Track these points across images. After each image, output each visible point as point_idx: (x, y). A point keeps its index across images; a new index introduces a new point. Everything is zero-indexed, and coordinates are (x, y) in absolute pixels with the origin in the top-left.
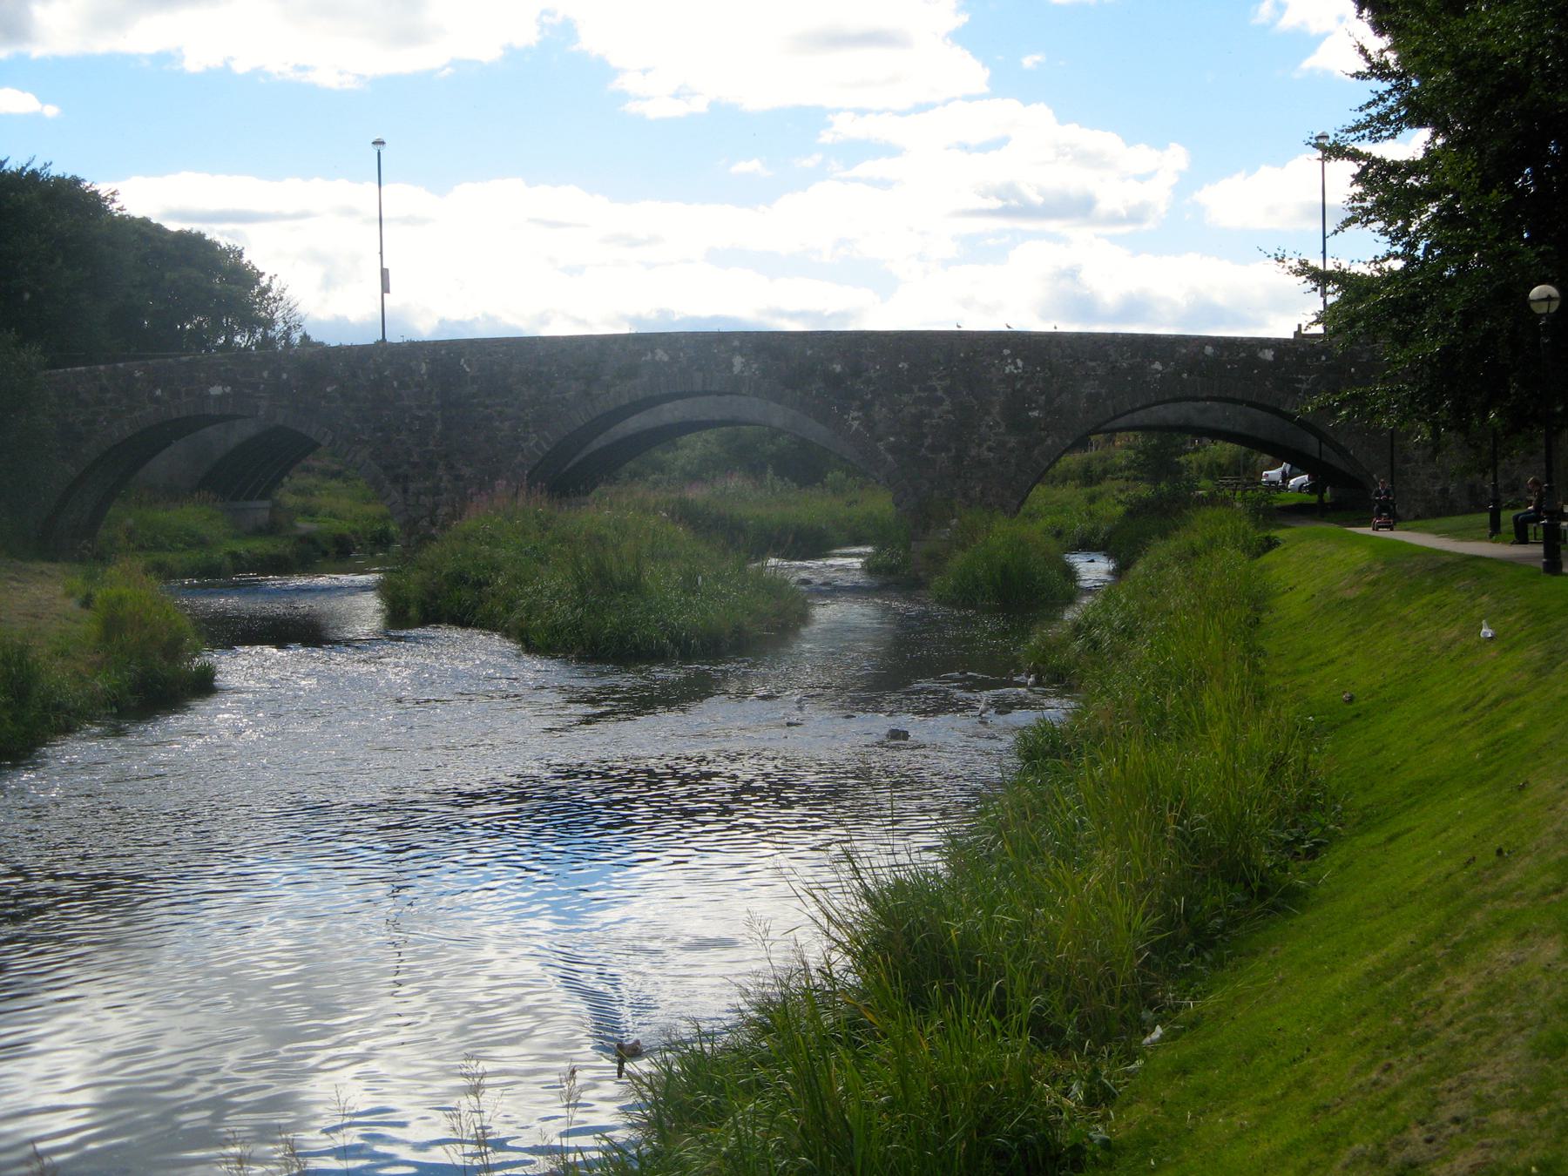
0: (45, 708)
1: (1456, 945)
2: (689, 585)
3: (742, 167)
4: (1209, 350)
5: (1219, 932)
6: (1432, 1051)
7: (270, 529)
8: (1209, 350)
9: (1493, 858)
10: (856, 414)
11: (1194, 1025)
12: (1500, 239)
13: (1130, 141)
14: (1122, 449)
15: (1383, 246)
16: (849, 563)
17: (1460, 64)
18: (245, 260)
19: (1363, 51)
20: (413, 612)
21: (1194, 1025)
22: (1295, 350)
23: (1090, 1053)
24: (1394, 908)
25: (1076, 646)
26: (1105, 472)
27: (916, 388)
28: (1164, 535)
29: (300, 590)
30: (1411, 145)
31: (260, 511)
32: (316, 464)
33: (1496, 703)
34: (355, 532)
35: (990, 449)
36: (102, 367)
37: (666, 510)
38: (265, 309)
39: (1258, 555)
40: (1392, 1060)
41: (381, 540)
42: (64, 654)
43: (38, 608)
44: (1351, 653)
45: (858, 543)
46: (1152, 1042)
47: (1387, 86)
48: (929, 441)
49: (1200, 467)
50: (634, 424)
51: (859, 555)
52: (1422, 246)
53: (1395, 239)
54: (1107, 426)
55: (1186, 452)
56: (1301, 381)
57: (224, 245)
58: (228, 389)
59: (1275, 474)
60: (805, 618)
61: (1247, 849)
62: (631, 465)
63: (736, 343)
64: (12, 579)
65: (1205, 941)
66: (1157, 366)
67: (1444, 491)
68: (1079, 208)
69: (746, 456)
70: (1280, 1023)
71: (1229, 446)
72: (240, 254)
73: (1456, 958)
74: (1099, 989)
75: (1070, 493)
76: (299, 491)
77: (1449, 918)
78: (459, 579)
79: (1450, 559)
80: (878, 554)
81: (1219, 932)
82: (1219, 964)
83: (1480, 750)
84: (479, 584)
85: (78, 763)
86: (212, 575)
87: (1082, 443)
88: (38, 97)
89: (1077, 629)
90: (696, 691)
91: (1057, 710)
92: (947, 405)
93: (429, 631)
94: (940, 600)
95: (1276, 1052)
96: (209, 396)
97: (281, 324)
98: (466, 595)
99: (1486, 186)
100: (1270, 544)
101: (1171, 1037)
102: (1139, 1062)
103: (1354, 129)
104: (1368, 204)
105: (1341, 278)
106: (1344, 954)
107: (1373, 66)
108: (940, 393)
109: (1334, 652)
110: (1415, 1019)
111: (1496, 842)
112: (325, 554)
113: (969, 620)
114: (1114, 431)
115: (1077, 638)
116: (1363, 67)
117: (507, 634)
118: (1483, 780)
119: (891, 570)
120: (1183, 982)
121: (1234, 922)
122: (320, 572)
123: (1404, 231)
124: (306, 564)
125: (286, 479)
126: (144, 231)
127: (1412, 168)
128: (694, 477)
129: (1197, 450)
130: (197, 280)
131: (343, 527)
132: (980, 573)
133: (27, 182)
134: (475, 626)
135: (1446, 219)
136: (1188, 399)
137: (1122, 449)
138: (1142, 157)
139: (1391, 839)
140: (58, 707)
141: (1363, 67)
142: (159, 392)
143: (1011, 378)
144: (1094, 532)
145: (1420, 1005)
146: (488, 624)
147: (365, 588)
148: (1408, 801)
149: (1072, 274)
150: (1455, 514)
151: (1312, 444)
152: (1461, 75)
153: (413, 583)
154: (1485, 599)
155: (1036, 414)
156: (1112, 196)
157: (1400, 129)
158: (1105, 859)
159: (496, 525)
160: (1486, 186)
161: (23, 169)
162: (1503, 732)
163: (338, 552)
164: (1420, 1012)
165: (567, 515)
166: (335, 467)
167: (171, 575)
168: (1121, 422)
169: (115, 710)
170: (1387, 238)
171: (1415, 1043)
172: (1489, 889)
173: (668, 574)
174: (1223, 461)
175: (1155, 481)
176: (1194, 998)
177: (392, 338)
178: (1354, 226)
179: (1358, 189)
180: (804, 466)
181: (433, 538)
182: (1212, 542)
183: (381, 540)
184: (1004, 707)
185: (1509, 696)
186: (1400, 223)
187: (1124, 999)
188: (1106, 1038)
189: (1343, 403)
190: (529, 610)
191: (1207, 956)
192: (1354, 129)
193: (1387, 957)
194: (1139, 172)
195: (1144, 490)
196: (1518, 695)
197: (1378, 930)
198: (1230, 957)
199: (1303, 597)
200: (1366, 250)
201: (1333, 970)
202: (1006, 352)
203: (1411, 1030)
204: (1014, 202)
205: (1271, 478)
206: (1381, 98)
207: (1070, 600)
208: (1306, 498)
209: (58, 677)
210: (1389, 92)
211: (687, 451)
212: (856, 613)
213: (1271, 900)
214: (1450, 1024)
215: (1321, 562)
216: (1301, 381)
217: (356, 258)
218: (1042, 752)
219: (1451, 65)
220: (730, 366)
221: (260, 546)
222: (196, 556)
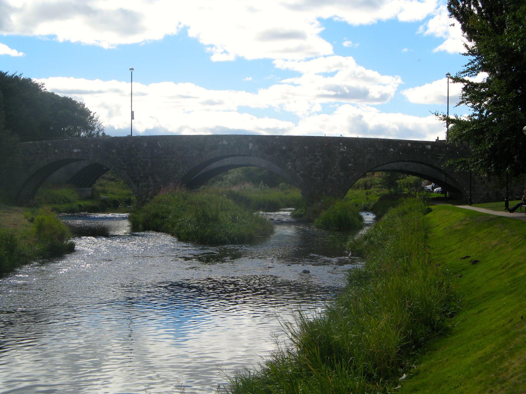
0: (19, 256)
1: (511, 349)
2: (234, 220)
3: (247, 79)
4: (409, 145)
5: (423, 342)
6: (507, 386)
7: (91, 198)
8: (409, 145)
9: (520, 320)
10: (290, 163)
11: (417, 374)
12: (512, 110)
13: (382, 74)
14: (377, 177)
15: (471, 111)
16: (285, 214)
17: (499, 50)
18: (85, 107)
19: (466, 46)
20: (140, 226)
21: (417, 374)
22: (438, 144)
23: (382, 382)
24: (485, 335)
25: (366, 243)
26: (372, 185)
27: (310, 155)
28: (394, 207)
29: (102, 218)
30: (482, 77)
31: (88, 191)
32: (106, 176)
33: (514, 266)
34: (120, 199)
35: (335, 176)
36: (38, 142)
37: (226, 194)
38: (92, 124)
39: (425, 214)
40: (493, 389)
41: (129, 202)
42: (25, 238)
43: (16, 222)
44: (460, 248)
45: (289, 207)
46: (402, 379)
47: (474, 58)
48: (314, 173)
49: (404, 184)
50: (215, 165)
51: (290, 211)
52: (485, 111)
53: (476, 109)
54: (374, 170)
55: (399, 179)
56: (440, 156)
57: (78, 102)
58: (80, 150)
59: (429, 187)
60: (272, 232)
61: (431, 314)
62: (212, 179)
63: (250, 139)
64: (7, 212)
65: (419, 345)
66: (392, 150)
67: (488, 194)
68: (361, 95)
69: (251, 178)
70: (449, 374)
71: (413, 177)
72: (84, 105)
73: (512, 354)
74: (384, 361)
75: (361, 193)
76: (101, 185)
77: (506, 340)
78: (156, 216)
79: (491, 217)
80: (296, 210)
81: (423, 342)
82: (424, 353)
83: (509, 282)
84: (163, 218)
85: (24, 276)
86: (73, 212)
87: (364, 176)
88: (17, 50)
89: (366, 238)
90: (236, 256)
91: (360, 265)
92: (321, 161)
93: (146, 233)
94: (318, 227)
95: (449, 385)
96: (73, 152)
97: (97, 129)
98: (159, 221)
99: (508, 91)
100: (430, 211)
101: (409, 378)
102: (399, 386)
103: (463, 72)
104: (468, 97)
105: (457, 122)
106: (469, 351)
107: (470, 51)
108: (318, 157)
109: (454, 247)
110: (499, 375)
111: (520, 314)
112: (110, 206)
113: (327, 234)
114: (374, 172)
115: (366, 240)
116: (466, 51)
117: (172, 235)
118: (511, 293)
119: (301, 216)
120: (411, 359)
121: (428, 339)
122: (108, 212)
123: (479, 106)
124: (103, 210)
125: (97, 181)
126: (52, 97)
127: (483, 85)
128: (235, 184)
129: (403, 178)
130: (70, 114)
131: (116, 197)
132: (331, 218)
133: (15, 80)
134: (161, 232)
135: (494, 103)
136: (402, 161)
137: (377, 177)
138: (386, 79)
139: (480, 312)
140: (23, 256)
141: (466, 51)
142: (56, 151)
143: (343, 153)
144: (369, 205)
145: (500, 370)
146: (166, 231)
147: (124, 218)
148: (485, 299)
149: (361, 117)
150: (491, 202)
151: (443, 177)
152: (500, 54)
153: (141, 217)
154: (506, 231)
155: (350, 165)
156: (374, 91)
157: (479, 72)
158: (385, 317)
159: (169, 197)
160: (508, 91)
161: (13, 75)
162: (517, 276)
163: (113, 206)
164: (500, 372)
165: (182, 192)
166: (113, 177)
167: (60, 212)
168: (379, 168)
169: (41, 257)
170: (473, 109)
171: (501, 383)
172: (520, 330)
173: (227, 216)
174: (411, 182)
175: (389, 187)
176: (416, 365)
177: (133, 135)
178: (462, 104)
179: (464, 93)
180: (271, 181)
181: (148, 202)
182: (410, 209)
183: (129, 202)
184: (341, 263)
185: (518, 264)
186: (478, 104)
187: (393, 365)
188: (386, 378)
189: (458, 164)
190: (180, 226)
191: (419, 350)
192: (463, 72)
193: (485, 353)
194: (387, 84)
195: (386, 191)
196: (522, 264)
197: (480, 343)
198: (427, 351)
199: (442, 228)
200: (465, 113)
201: (465, 357)
202: (341, 144)
203: (498, 378)
204: (339, 93)
205: (428, 188)
206: (473, 62)
207: (361, 228)
208: (440, 195)
209: (23, 246)
210: (475, 60)
211: (232, 175)
212: (289, 231)
213: (440, 332)
214: (512, 376)
215: (446, 217)
216: (440, 156)
217: (123, 109)
218: (358, 279)
219: (497, 51)
220: (248, 146)
221: (88, 203)
222: (67, 206)
